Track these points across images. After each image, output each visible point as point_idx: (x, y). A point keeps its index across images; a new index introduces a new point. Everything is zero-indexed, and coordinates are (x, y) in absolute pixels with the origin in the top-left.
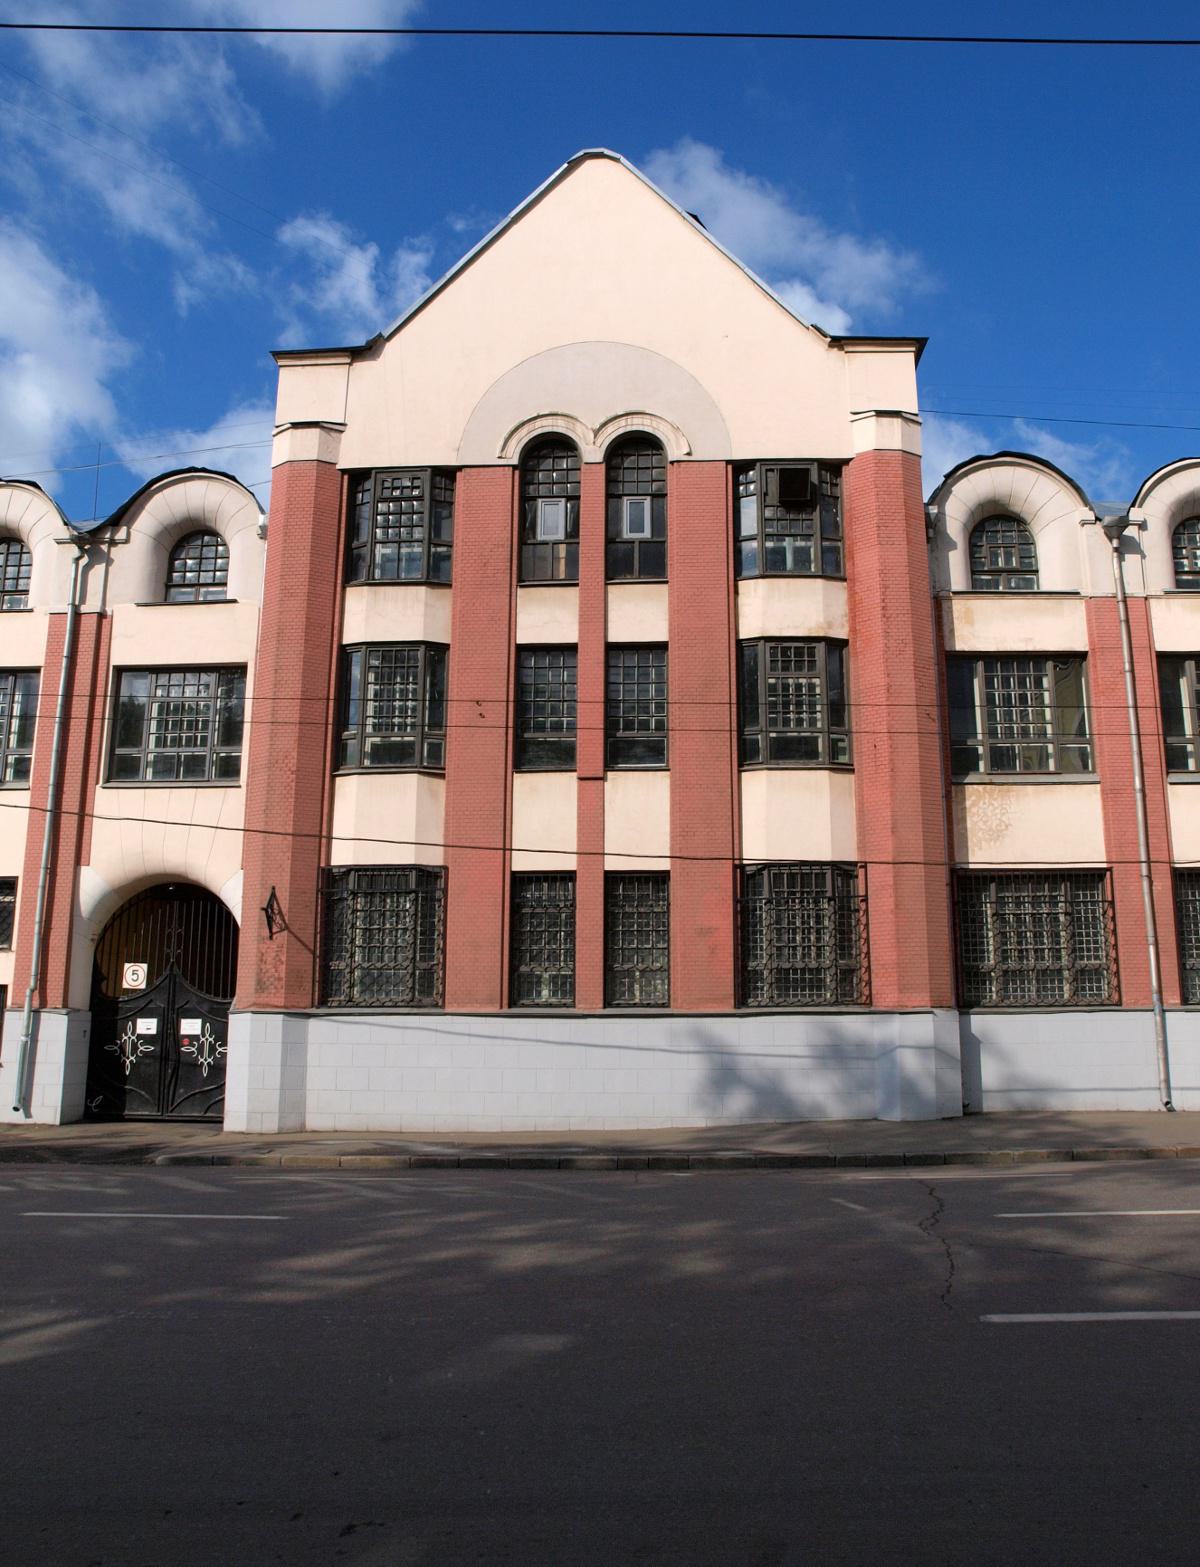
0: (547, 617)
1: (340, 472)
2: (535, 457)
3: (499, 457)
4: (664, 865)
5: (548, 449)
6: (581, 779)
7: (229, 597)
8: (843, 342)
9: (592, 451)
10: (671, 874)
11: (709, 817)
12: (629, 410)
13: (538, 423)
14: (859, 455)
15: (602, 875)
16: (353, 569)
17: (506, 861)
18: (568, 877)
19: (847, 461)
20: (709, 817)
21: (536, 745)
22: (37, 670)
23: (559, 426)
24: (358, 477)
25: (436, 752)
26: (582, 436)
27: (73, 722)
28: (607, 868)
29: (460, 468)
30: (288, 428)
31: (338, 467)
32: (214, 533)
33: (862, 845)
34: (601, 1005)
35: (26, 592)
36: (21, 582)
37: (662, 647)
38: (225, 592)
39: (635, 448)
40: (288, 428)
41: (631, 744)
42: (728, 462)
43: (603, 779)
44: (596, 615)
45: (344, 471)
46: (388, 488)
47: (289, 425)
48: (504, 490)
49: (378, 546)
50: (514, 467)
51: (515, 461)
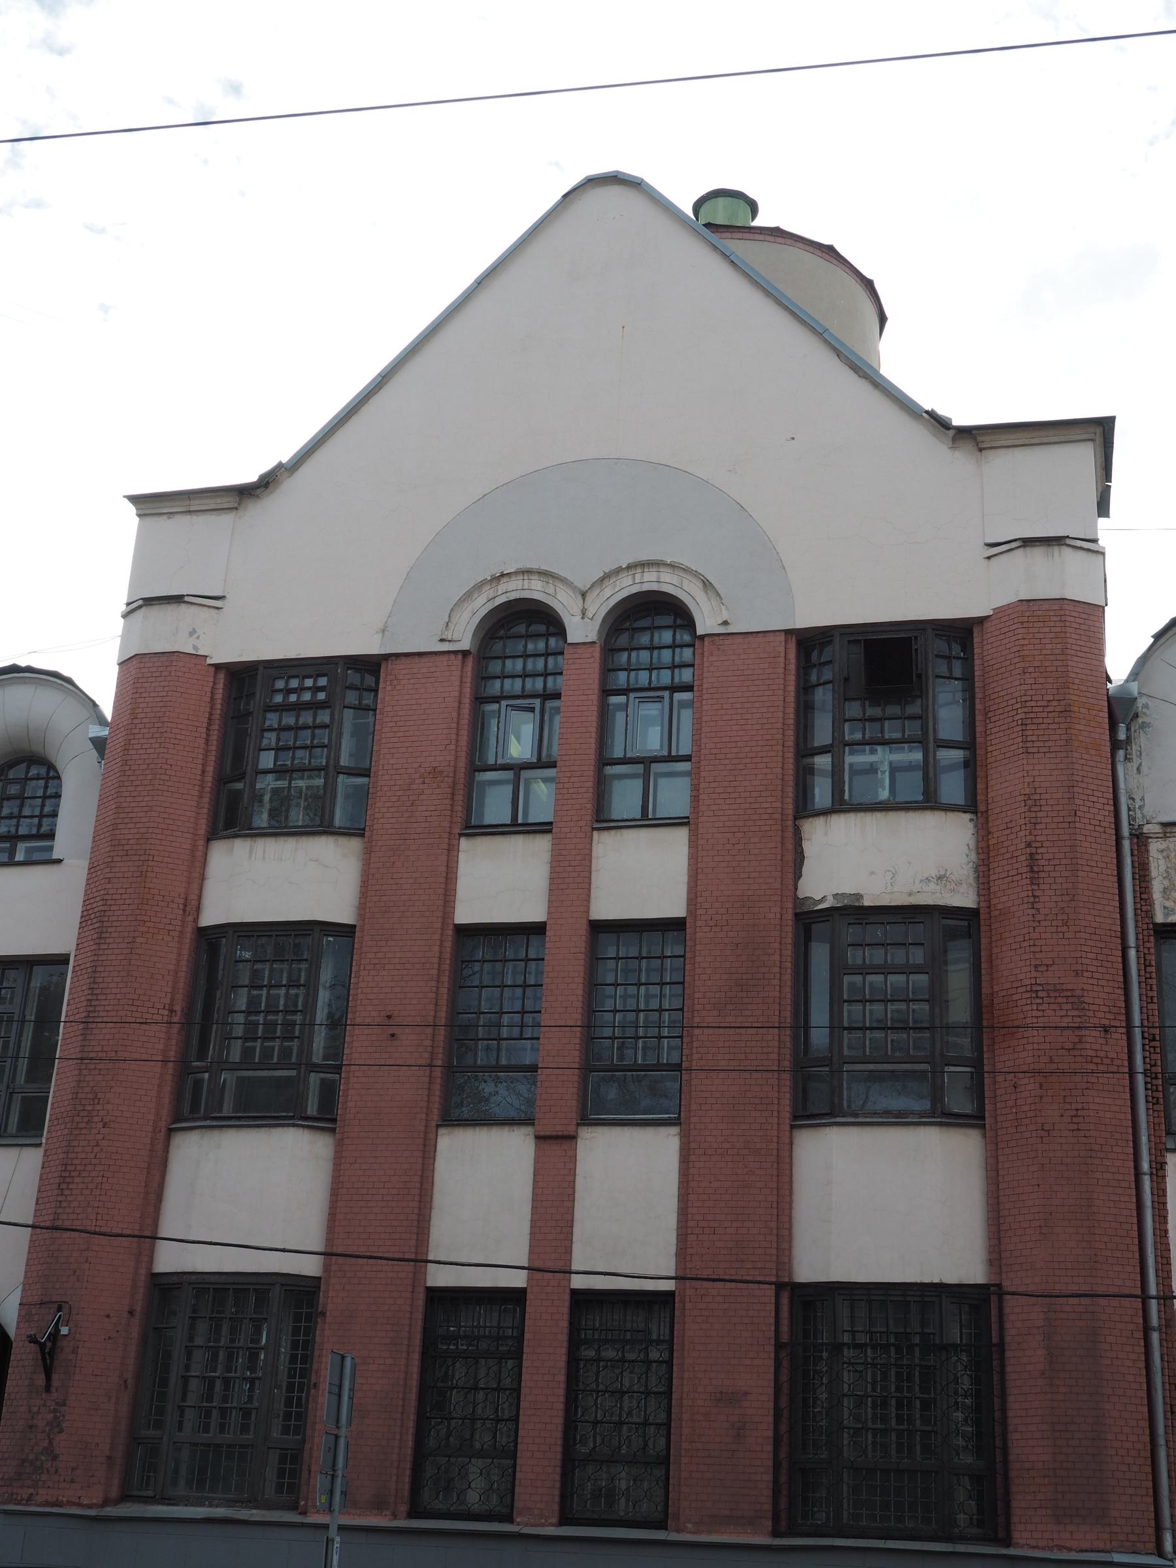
0: (500, 883)
1: (212, 669)
2: (501, 638)
3: (442, 640)
4: (517, 1280)
5: (520, 624)
6: (538, 1138)
7: (55, 856)
8: (987, 441)
9: (583, 627)
10: (529, 1296)
11: (734, 1206)
12: (644, 557)
13: (504, 586)
14: (997, 611)
15: (567, 1297)
16: (231, 817)
17: (419, 1274)
18: (516, 1297)
19: (981, 620)
20: (383, 1208)
21: (468, 1083)
22: (63, 960)
23: (535, 590)
24: (243, 680)
25: (329, 1095)
26: (564, 604)
27: (576, 1016)
28: (428, 1285)
29: (387, 657)
30: (140, 607)
31: (209, 661)
32: (51, 767)
33: (996, 1255)
34: (554, 1520)
35: (51, 836)
36: (46, 821)
37: (538, 929)
38: (51, 848)
39: (650, 616)
40: (140, 607)
41: (623, 1082)
42: (788, 632)
43: (573, 1138)
44: (571, 876)
45: (218, 667)
46: (281, 690)
47: (140, 602)
48: (451, 689)
49: (341, 776)
50: (465, 654)
51: (465, 644)
